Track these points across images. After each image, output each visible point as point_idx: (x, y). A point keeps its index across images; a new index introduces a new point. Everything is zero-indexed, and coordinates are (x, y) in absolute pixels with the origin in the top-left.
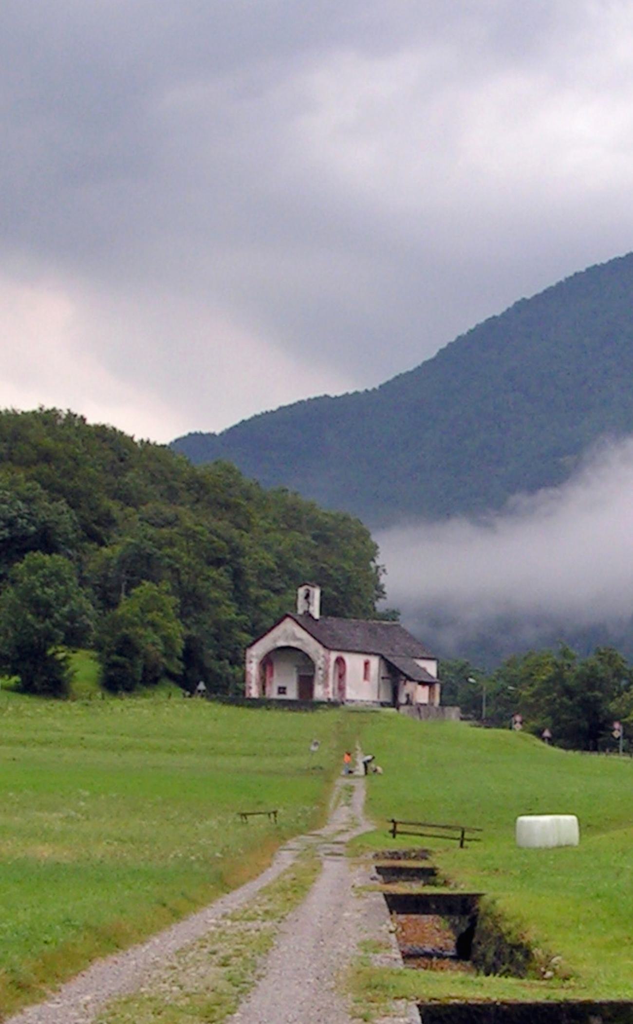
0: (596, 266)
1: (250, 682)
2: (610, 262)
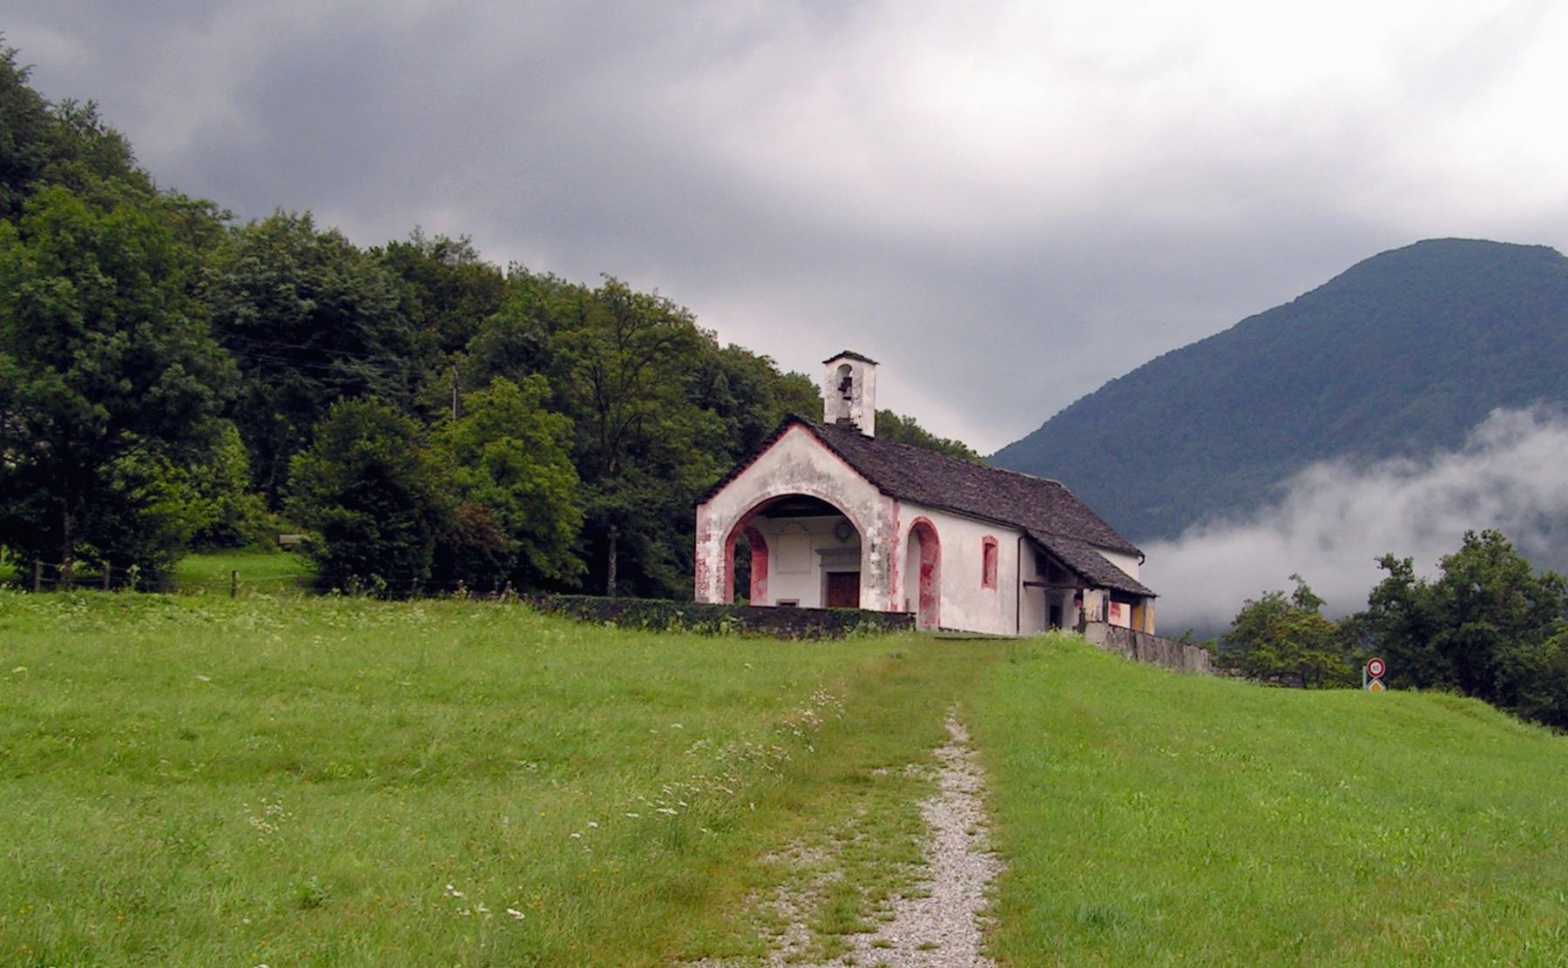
0: (1173, 351)
1: (707, 587)
2: (1186, 347)
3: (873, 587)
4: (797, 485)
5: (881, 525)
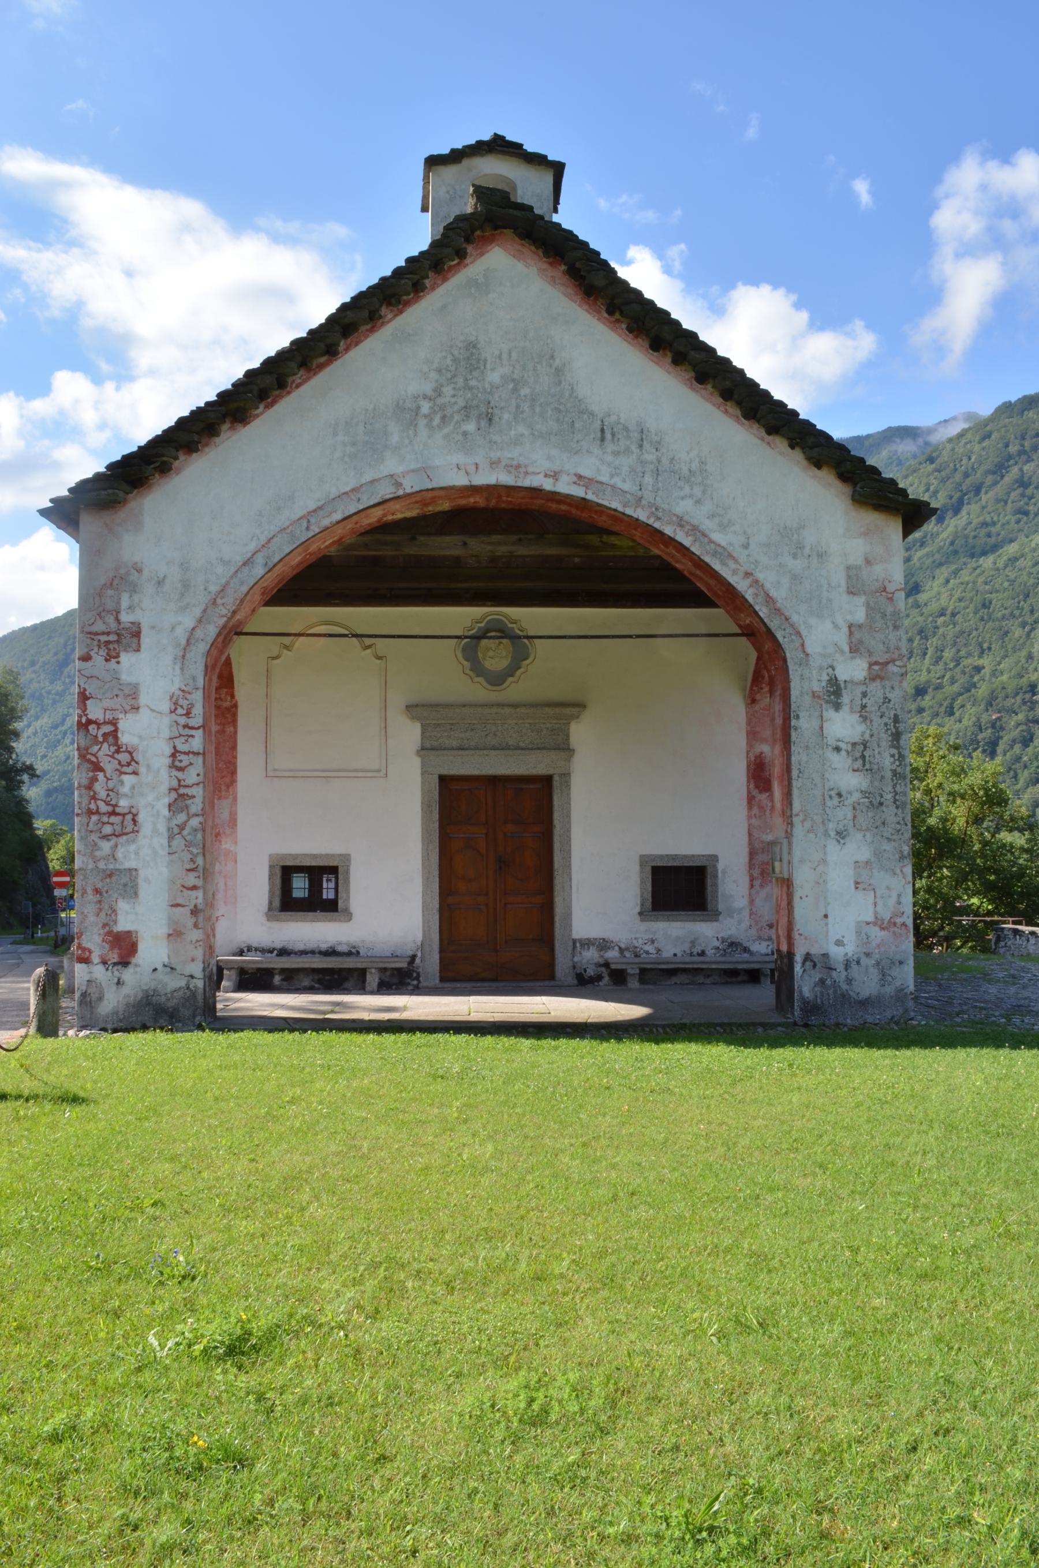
3: (841, 835)
4: (513, 453)
5: (860, 615)
